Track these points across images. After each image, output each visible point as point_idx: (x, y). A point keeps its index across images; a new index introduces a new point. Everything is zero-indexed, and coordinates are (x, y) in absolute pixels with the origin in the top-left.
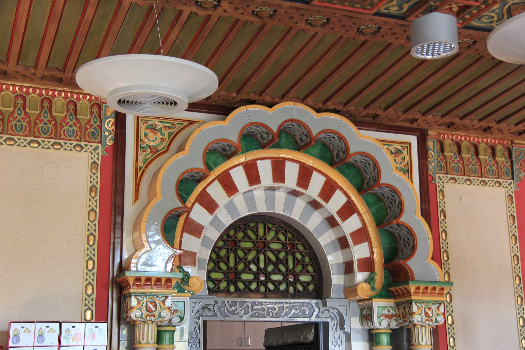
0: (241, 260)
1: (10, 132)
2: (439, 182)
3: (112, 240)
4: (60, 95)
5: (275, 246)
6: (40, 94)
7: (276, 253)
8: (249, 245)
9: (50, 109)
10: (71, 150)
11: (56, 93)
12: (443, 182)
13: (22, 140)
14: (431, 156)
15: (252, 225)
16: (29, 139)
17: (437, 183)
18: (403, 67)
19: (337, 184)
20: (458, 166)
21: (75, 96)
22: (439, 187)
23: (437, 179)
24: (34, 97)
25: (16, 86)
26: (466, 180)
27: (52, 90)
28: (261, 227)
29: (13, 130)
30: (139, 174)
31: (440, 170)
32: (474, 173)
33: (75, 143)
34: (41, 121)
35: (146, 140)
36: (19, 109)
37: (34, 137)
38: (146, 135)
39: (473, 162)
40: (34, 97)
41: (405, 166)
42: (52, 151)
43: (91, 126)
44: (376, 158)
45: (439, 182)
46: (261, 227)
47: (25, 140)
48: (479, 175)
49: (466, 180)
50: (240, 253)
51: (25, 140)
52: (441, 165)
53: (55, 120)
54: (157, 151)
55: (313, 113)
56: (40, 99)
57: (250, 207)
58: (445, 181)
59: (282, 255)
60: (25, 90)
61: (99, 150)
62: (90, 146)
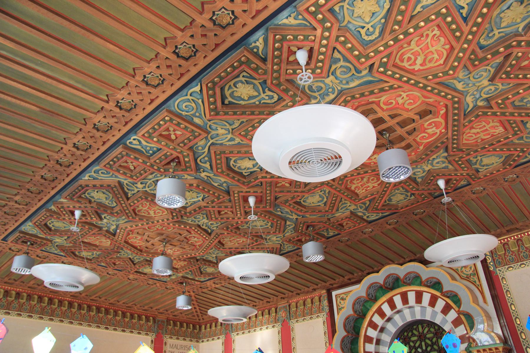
0: (435, 343)
1: (508, 263)
2: (500, 273)
3: (506, 324)
4: (525, 235)
5: (429, 336)
6: (515, 239)
7: (431, 339)
8: (428, 336)
9: (523, 244)
10: (518, 268)
11: (522, 235)
12: (503, 272)
13: (516, 266)
14: (488, 259)
15: (415, 327)
16: (519, 264)
17: (499, 274)
18: (206, 310)
19: (437, 296)
20: (512, 258)
21: (519, 236)
22: (501, 276)
23: (498, 272)
24: (511, 241)
25: (514, 236)
26: (521, 264)
27: (526, 232)
28: (420, 327)
29: (509, 262)
30: (480, 288)
31: (499, 265)
32: (526, 258)
33: (317, 315)
34: (521, 252)
35: (340, 305)
36: (508, 250)
37: (521, 262)
38: (340, 303)
39: (524, 251)
40: (511, 241)
41: (473, 271)
42: (521, 269)
43: (508, 256)
44: (438, 278)
45: (500, 273)
46: (420, 327)
47: (517, 265)
48: (503, 264)
49: (521, 264)
50: (412, 344)
51: (517, 265)
52: (499, 262)
53: (528, 249)
54: (468, 278)
55: (399, 266)
56: (515, 241)
57: (412, 316)
58: (504, 271)
59: (434, 340)
60: (506, 240)
61: (325, 315)
62: (321, 315)
